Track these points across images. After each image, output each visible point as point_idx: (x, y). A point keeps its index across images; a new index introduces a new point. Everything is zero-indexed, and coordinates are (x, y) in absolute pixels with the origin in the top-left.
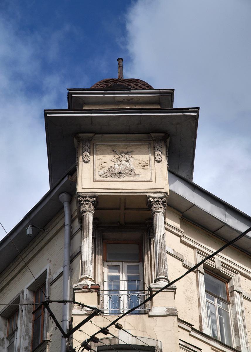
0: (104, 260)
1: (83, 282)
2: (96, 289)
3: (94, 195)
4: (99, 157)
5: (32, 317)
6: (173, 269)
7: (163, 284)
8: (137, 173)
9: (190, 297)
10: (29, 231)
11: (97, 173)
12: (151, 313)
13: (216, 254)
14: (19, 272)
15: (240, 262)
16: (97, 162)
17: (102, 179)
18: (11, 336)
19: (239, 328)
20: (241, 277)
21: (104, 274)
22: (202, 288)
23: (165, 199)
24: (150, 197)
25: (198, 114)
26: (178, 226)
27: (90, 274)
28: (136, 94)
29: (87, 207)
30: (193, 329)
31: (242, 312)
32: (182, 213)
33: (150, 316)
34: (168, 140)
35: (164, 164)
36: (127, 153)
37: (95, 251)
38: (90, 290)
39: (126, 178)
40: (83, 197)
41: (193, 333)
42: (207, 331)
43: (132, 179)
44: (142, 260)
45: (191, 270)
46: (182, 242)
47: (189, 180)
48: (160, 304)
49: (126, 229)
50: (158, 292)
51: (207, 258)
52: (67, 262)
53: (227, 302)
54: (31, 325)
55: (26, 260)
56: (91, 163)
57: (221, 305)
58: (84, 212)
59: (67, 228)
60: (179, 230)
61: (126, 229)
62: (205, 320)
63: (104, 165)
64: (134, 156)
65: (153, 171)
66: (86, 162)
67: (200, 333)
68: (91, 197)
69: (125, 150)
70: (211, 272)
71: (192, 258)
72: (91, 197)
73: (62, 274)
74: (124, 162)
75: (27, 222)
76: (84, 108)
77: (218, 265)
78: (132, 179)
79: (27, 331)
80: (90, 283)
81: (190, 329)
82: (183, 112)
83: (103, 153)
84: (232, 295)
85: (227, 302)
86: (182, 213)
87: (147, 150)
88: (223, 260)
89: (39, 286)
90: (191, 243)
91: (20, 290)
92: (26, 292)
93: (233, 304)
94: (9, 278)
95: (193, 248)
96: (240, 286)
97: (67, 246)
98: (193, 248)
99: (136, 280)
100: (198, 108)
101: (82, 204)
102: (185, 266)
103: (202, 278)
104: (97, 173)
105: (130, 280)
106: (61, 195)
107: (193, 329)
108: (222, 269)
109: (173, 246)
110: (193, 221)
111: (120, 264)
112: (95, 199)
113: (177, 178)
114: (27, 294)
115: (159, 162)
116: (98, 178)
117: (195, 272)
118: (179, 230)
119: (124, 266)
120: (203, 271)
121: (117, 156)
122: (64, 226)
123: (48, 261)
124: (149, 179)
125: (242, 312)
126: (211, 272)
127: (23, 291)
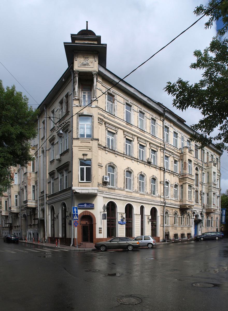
0: (82, 90)
1: (75, 98)
2: (78, 100)
3: (78, 71)
4: (80, 59)
5: (66, 104)
6: (98, 93)
7: (95, 99)
8: (90, 65)
9: (103, 101)
10: (63, 80)
11: (80, 64)
12: (92, 107)
13: (110, 89)
14: (63, 91)
15: (117, 91)
16: (79, 61)
17: (80, 66)
18: (62, 108)
19: (45, 210)
20: (117, 95)
21: (82, 94)
22: (107, 99)
23: (96, 74)
24: (93, 73)
25: (106, 46)
26: (101, 81)
27: (77, 95)
28: (91, 37)
29: (76, 75)
30: (103, 110)
31: (117, 105)
32: (102, 77)
33: (91, 107)
34: (99, 54)
35: (97, 62)
36: (87, 58)
37: (79, 87)
38: (77, 100)
39: (87, 66)
40: (75, 72)
41: (103, 111)
42: (107, 111)
43: (88, 67)
44: (91, 91)
45: (104, 93)
46: (102, 85)
47: (105, 67)
48: (94, 104)
49: (86, 81)
50: (94, 101)
51: (108, 90)
52: (73, 91)
53: (113, 102)
54: (66, 106)
55: (58, 96)
56: (77, 60)
57: (112, 103)
58: (75, 77)
59: (72, 80)
60: (101, 82)
61: (86, 81)
62: (107, 108)
63: (81, 62)
64: (89, 59)
65: (94, 64)
66: (76, 61)
67: (105, 111)
68: (77, 72)
69: (87, 57)
70: (109, 94)
71: (104, 90)
72: (77, 72)
73: (71, 94)
74: (86, 61)
75: (63, 77)
76: (76, 42)
77: (111, 92)
78: (88, 67)
79: (65, 108)
80: (77, 98)
81: (102, 110)
82: (102, 45)
83: (81, 58)
84: (114, 101)
85: (113, 102)
86: (102, 77)
87: (93, 57)
88: (113, 90)
89: (67, 96)
90: (105, 86)
91: (63, 97)
92: (64, 97)
93: (115, 103)
94: (61, 92)
95: (105, 87)
96: (117, 98)
97: (73, 86)
98: (105, 87)
99: (90, 97)
100: (106, 44)
101: (75, 74)
102: (102, 93)
103: (107, 96)
104: (80, 64)
105: (88, 96)
106: (71, 70)
107: (103, 110)
108: (112, 93)
109: (100, 87)
110: (106, 79)
111: (86, 91)
112: (78, 73)
113: (101, 66)
114: (65, 98)
115: (96, 61)
116: (79, 66)
117: (105, 94)
118: (101, 82)
119: (87, 92)
120: (107, 94)
121: (84, 59)
122: (72, 80)
123: (68, 90)
124: (92, 67)
125: (117, 105)
126: (109, 94)
127: (64, 97)
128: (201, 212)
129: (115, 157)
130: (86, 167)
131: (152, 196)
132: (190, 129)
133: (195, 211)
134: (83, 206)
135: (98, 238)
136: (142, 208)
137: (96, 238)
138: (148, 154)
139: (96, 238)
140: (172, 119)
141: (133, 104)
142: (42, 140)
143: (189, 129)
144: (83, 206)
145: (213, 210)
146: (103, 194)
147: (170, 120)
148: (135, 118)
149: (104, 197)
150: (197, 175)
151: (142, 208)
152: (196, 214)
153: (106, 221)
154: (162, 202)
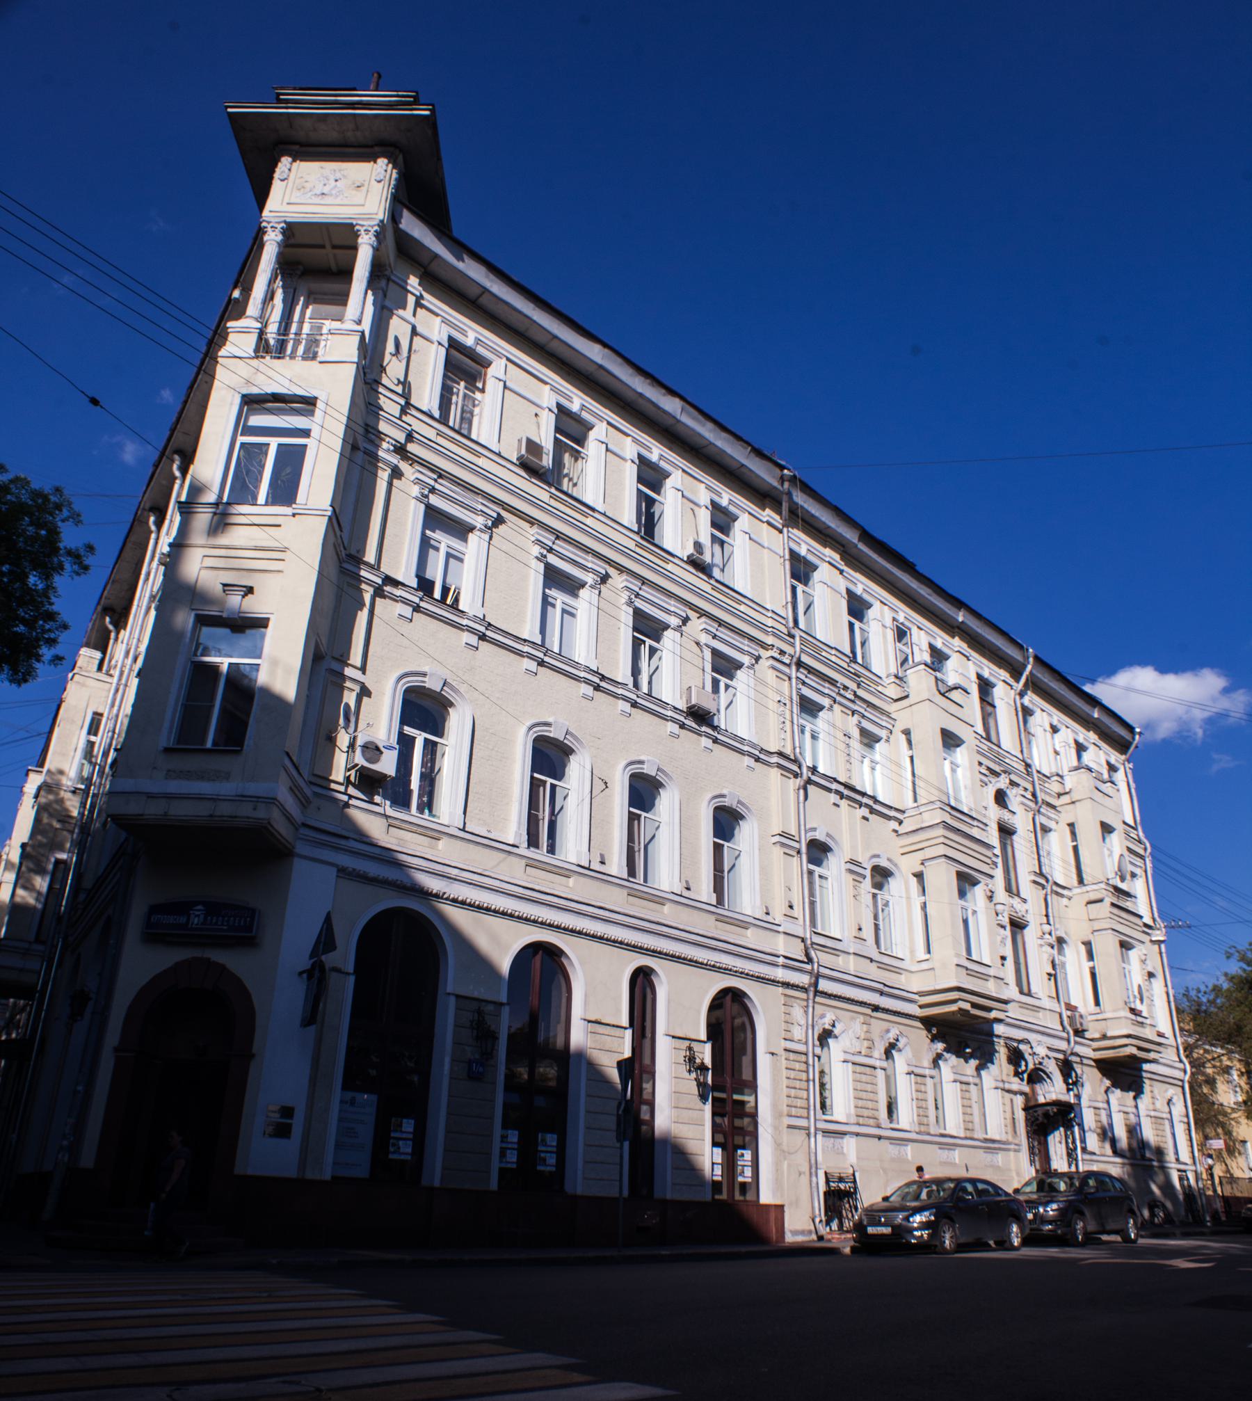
128: (1061, 1056)
129: (65, 492)
130: (426, 740)
131: (532, 864)
132: (935, 592)
133: (1022, 1047)
134: (183, 920)
135: (250, 1172)
136: (642, 982)
137: (238, 1170)
138: (676, 672)
139: (238, 1170)
140: (829, 527)
141: (676, 466)
142: (1018, 895)
143: (929, 591)
144: (183, 920)
145: (1140, 1048)
146: (337, 849)
147: (820, 532)
148: (682, 525)
149: (343, 872)
150: (1006, 831)
151: (642, 982)
152: (1031, 1066)
153: (708, 1107)
154: (791, 963)
